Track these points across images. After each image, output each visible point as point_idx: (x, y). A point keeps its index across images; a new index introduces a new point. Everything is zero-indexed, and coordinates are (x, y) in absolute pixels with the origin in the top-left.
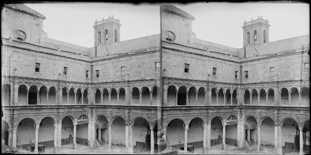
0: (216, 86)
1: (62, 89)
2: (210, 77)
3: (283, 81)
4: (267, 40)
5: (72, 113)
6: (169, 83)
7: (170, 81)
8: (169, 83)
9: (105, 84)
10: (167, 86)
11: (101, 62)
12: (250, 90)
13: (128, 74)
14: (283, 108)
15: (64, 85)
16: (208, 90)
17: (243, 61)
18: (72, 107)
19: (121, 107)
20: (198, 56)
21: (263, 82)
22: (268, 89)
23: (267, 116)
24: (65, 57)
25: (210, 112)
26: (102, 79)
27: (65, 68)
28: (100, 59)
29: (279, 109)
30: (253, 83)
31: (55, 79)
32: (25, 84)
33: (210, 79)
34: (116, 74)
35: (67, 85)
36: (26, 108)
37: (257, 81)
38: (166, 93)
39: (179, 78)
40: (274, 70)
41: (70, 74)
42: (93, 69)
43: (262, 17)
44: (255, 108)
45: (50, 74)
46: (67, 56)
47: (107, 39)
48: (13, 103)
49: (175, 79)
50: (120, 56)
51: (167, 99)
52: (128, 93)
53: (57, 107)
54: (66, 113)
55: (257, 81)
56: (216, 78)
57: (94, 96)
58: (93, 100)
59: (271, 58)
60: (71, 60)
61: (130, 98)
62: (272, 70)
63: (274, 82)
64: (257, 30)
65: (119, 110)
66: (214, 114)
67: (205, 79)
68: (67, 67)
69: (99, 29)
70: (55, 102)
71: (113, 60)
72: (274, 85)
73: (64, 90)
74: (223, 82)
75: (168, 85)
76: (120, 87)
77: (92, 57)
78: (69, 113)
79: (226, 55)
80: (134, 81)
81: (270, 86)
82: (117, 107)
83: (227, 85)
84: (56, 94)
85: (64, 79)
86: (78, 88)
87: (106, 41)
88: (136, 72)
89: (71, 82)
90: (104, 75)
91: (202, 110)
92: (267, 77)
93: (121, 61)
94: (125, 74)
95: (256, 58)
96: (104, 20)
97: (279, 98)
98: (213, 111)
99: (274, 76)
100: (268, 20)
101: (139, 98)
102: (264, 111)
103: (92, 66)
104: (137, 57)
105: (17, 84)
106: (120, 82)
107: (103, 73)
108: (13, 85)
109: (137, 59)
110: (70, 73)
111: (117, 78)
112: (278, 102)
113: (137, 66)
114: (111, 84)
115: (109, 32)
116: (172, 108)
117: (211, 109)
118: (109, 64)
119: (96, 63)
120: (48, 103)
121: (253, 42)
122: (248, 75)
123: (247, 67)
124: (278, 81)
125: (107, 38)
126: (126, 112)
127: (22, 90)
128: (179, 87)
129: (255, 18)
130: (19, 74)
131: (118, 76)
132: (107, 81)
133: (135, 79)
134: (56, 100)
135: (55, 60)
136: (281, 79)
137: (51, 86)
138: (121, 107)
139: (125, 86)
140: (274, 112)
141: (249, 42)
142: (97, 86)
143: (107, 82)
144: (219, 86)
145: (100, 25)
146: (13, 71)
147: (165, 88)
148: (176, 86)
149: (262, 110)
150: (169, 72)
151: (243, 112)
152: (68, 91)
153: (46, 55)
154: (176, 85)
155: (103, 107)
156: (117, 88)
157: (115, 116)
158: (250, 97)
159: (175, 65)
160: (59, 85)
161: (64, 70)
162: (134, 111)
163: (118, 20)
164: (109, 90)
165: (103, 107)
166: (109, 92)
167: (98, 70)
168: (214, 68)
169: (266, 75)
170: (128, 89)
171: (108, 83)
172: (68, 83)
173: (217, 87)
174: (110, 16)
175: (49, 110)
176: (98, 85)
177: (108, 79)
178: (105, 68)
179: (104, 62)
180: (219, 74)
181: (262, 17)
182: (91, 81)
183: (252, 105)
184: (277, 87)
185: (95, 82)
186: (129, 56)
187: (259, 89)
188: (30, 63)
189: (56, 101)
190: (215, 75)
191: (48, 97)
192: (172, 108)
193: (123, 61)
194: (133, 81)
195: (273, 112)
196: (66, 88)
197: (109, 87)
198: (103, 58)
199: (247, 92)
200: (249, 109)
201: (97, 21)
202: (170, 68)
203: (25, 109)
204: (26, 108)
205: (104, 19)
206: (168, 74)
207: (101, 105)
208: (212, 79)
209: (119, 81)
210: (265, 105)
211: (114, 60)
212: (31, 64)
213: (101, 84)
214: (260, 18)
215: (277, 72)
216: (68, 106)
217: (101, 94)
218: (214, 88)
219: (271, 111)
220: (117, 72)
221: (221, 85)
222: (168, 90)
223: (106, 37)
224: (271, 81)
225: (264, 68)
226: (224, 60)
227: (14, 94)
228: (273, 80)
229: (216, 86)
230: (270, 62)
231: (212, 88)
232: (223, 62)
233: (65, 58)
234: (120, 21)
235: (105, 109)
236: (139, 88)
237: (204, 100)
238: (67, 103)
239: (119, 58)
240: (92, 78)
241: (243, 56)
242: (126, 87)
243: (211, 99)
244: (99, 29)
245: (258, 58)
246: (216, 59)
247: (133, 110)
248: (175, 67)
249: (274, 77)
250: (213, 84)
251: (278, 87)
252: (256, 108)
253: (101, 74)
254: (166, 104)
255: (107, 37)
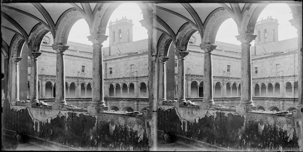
0: (230, 81)
1: (81, 85)
2: (225, 74)
3: (287, 76)
4: (276, 38)
5: (235, 104)
6: (192, 79)
7: (193, 77)
8: (192, 79)
9: (262, 79)
10: (45, 82)
11: (259, 60)
12: (114, 85)
13: (136, 71)
14: (288, 99)
15: (82, 81)
16: (223, 84)
17: (108, 59)
18: (89, 100)
19: (276, 99)
20: (69, 56)
21: (125, 77)
22: (129, 83)
23: (128, 106)
24: (228, 57)
25: (80, 103)
26: (260, 75)
27: (229, 66)
28: (113, 58)
29: (284, 100)
30: (262, 78)
31: (220, 76)
32: (196, 80)
33: (225, 75)
34: (127, 71)
35: (84, 81)
36: (52, 100)
37: (120, 77)
38: (190, 87)
39: (199, 75)
40: (134, 67)
41: (88, 72)
42: (107, 67)
43: (126, 17)
44: (264, 100)
45: (71, 72)
46: (230, 56)
47: (121, 38)
48: (42, 96)
49: (197, 76)
50: (130, 55)
51: (45, 93)
52: (136, 87)
53: (222, 99)
54: (84, 105)
55: (120, 77)
56: (85, 74)
57: (108, 90)
58: (107, 93)
59: (277, 56)
60: (233, 59)
61: (138, 91)
62: (132, 68)
63: (134, 77)
64: (121, 29)
65: (130, 102)
66: (83, 105)
67: (75, 75)
68: (84, 66)
69: (259, 29)
70: (75, 95)
71: (124, 59)
72: (134, 80)
73: (228, 84)
74: (236, 77)
75: (46, 81)
76: (131, 82)
77: (106, 56)
78: (86, 105)
79: (239, 54)
80: (142, 77)
81: (276, 80)
82: (128, 100)
83: (234, 79)
84: (76, 88)
85: (83, 76)
86: (88, 83)
87: (120, 40)
88: (143, 70)
89: (234, 78)
90: (262, 72)
91: (73, 101)
92: (273, 72)
93: (130, 60)
94: (134, 71)
95: (264, 56)
96: (117, 21)
97: (138, 90)
98: (228, 102)
99: (134, 72)
100: (277, 20)
101: (127, 92)
102: (271, 102)
103: (106, 64)
104: (144, 56)
105: (44, 81)
106: (275, 78)
107: (116, 70)
108: (41, 82)
109: (144, 58)
110: (88, 71)
111: (127, 75)
112: (138, 94)
113: (144, 64)
114: (122, 80)
115: (122, 31)
116: (49, 100)
117: (81, 100)
118: (121, 62)
119: (109, 62)
120: (69, 96)
121: (263, 40)
122: (258, 71)
123: (256, 64)
124: (137, 76)
125: (121, 37)
126: (135, 104)
127: (194, 85)
128: (200, 82)
129: (120, 18)
130: (192, 73)
131: (128, 73)
132: (119, 77)
133: (288, 75)
134: (76, 94)
135: (220, 60)
136: (140, 75)
137: (217, 82)
138: (276, 99)
139: (134, 81)
140: (280, 102)
141: (260, 40)
142: (111, 82)
143: (119, 78)
144: (232, 81)
145: (115, 25)
146: (187, 70)
147: (189, 84)
148: (52, 82)
149: (270, 101)
150: (191, 70)
151: (108, 104)
152: (231, 86)
153: (67, 56)
154: (52, 81)
155: (116, 99)
156: (127, 83)
157: (126, 107)
158: (260, 91)
159: (51, 65)
160: (78, 81)
161: (228, 68)
162: (142, 103)
163: (131, 20)
164: (267, 85)
165: (116, 99)
166: (121, 86)
167: (111, 68)
168: (82, 66)
169: (273, 71)
170: (136, 84)
171: (120, 78)
172: (85, 80)
173: (85, 82)
174: (123, 17)
175: (70, 102)
176: (257, 80)
177: (265, 75)
178: (262, 66)
179: (262, 60)
180: (233, 71)
181: (126, 17)
182: (106, 77)
183: (261, 97)
184: (282, 81)
185: (108, 78)
186: (283, 55)
187: (122, 83)
188: (200, 63)
189: (221, 94)
190: (83, 72)
191: (69, 91)
192: (49, 100)
193: (132, 60)
194: (141, 77)
195: (133, 103)
196: (84, 84)
197: (121, 82)
198: (115, 57)
199: (257, 86)
200: (259, 100)
201: (112, 22)
202: (47, 67)
203: (197, 101)
204: (52, 100)
205: (118, 20)
206: (191, 72)
207: (114, 97)
208: (227, 75)
209: (129, 77)
210: (126, 97)
211: (270, 59)
212: (201, 63)
213: (114, 80)
214: (124, 18)
215: (137, 68)
216: (231, 98)
217: (114, 88)
218: (83, 83)
219: (132, 102)
220: (127, 69)
221: (89, 81)
222: (46, 85)
223: (265, 35)
224: (131, 77)
225: (126, 65)
226: (236, 58)
227: (42, 89)
228: (279, 75)
229: (230, 81)
230: (276, 60)
231: (82, 83)
232: (235, 60)
233: (83, 58)
234: (278, 21)
235: (117, 101)
236: (291, 83)
237: (75, 93)
238: (85, 96)
239: (274, 57)
240: (106, 74)
241: (108, 54)
242: (135, 82)
243: (80, 92)
244: (114, 29)
245: (266, 56)
246: (230, 58)
247: (141, 102)
248: (197, 66)
249: (134, 73)
250: (83, 79)
251: (137, 81)
252: (264, 99)
253: (113, 71)
254: (45, 96)
255: (266, 36)
